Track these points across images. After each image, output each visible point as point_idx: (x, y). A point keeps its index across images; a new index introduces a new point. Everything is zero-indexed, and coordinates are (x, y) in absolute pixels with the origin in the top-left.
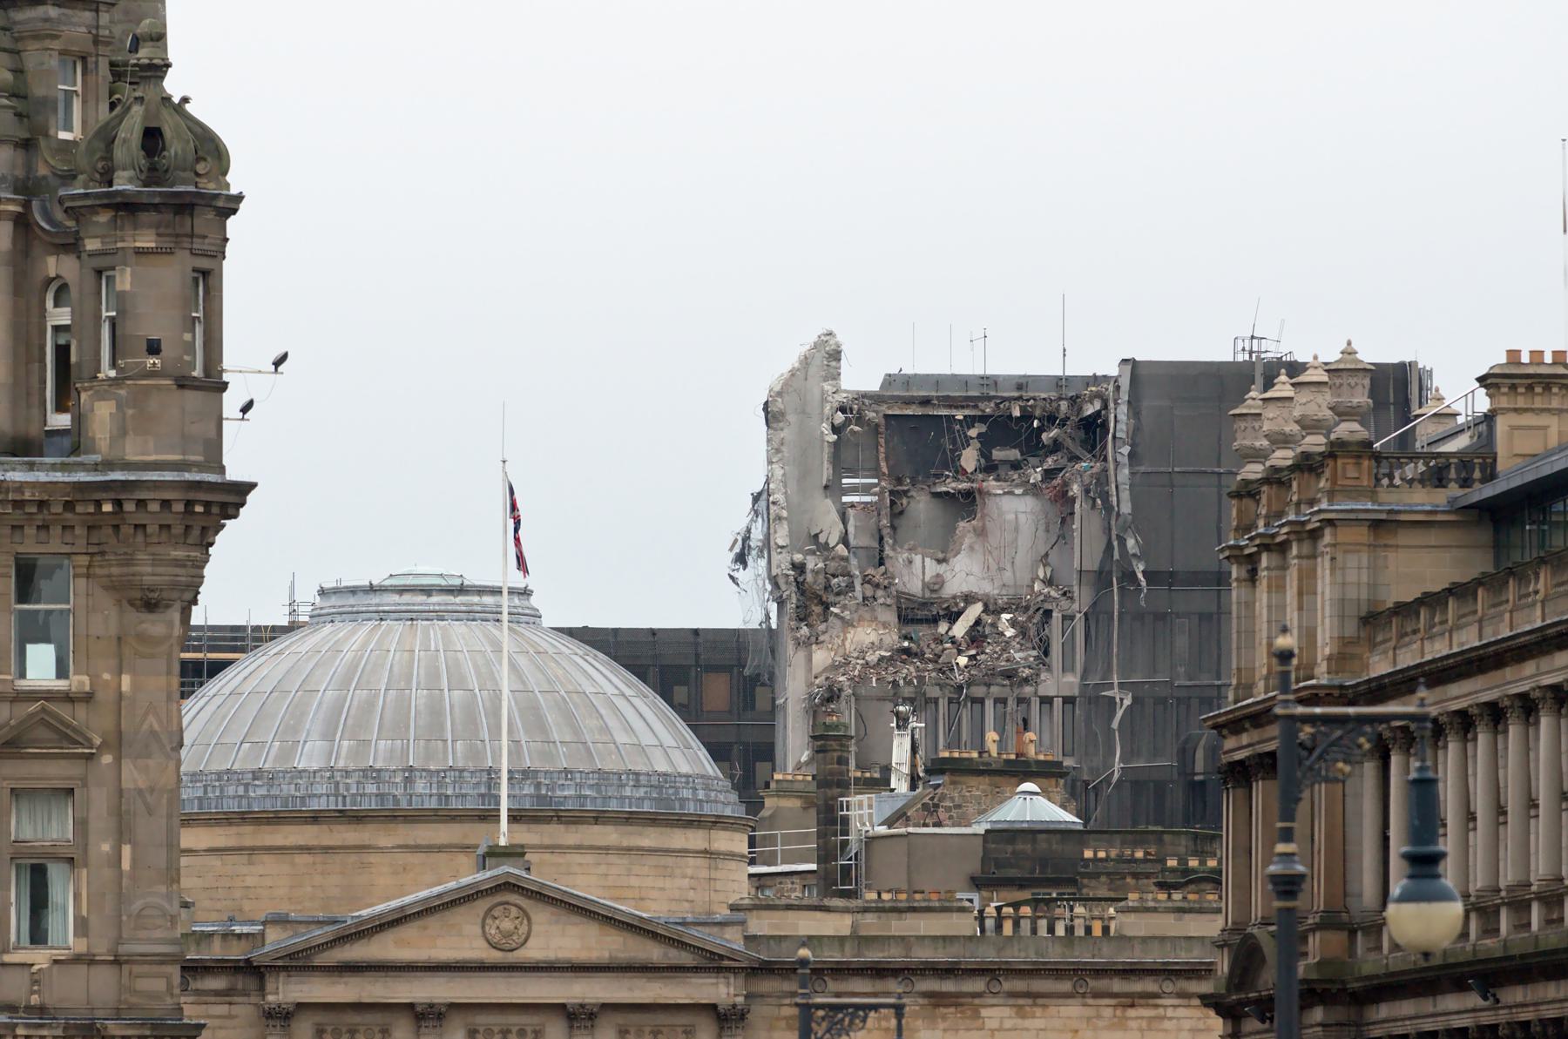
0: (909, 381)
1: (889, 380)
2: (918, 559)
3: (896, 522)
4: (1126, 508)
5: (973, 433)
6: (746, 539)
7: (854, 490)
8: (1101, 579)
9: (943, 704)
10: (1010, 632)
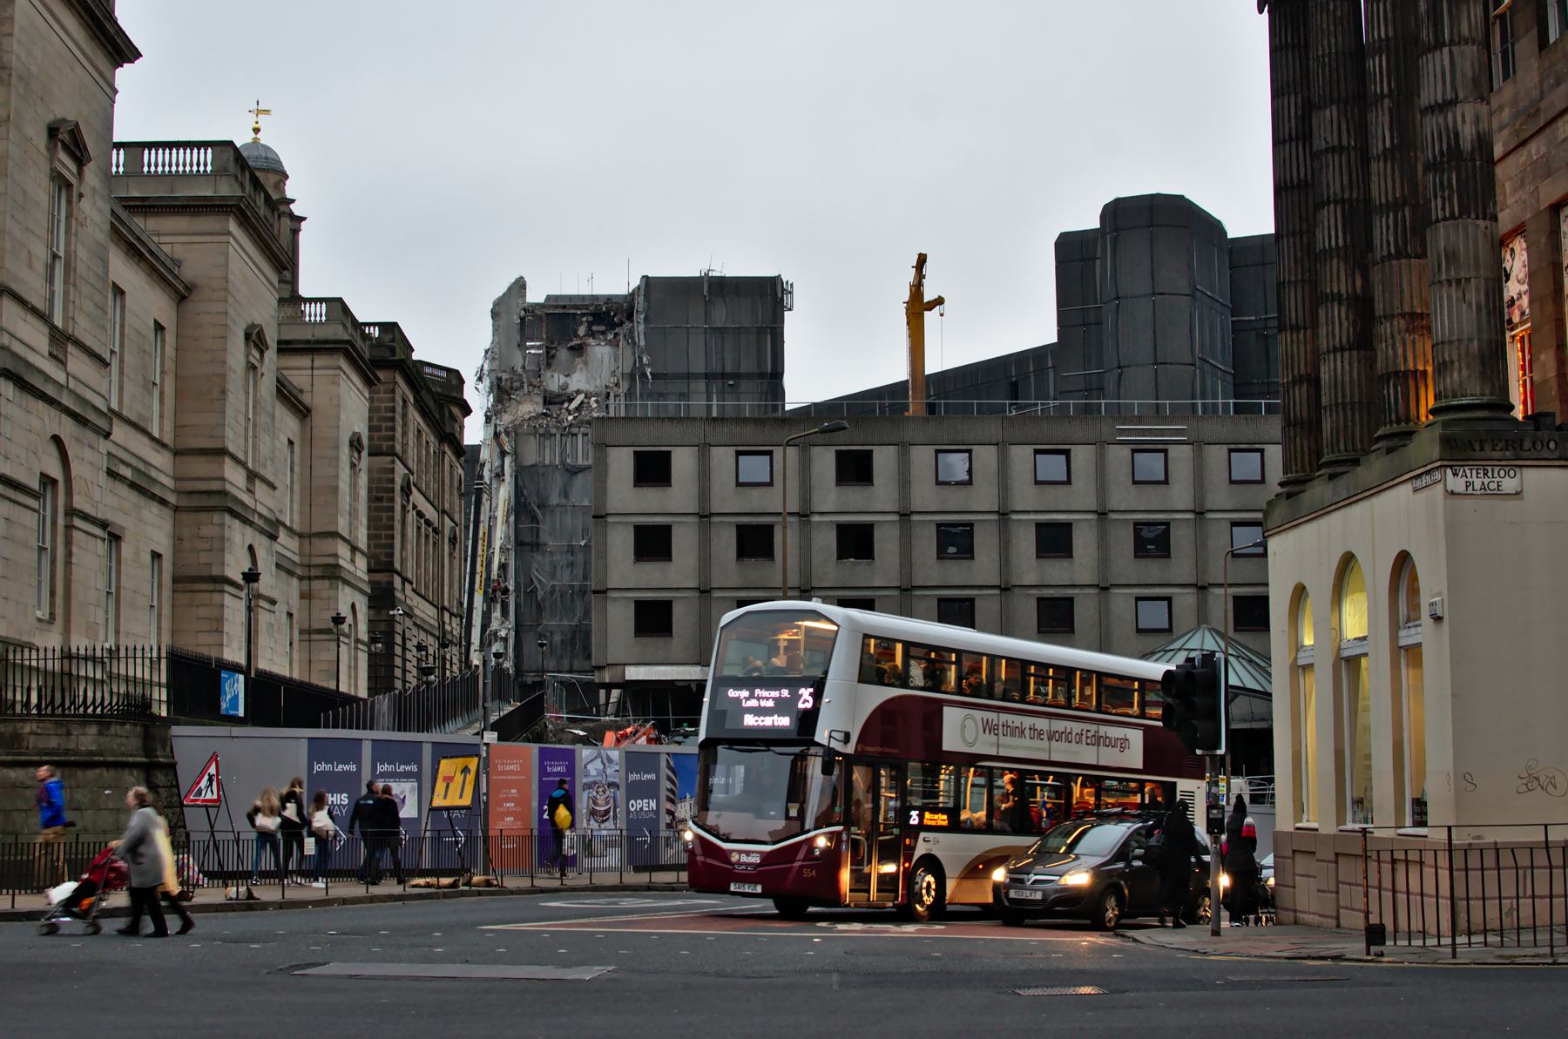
0: (557, 297)
1: (549, 297)
2: (556, 375)
3: (551, 361)
4: (642, 343)
5: (584, 319)
6: (482, 370)
7: (532, 347)
8: (632, 376)
9: (558, 436)
10: (595, 405)
